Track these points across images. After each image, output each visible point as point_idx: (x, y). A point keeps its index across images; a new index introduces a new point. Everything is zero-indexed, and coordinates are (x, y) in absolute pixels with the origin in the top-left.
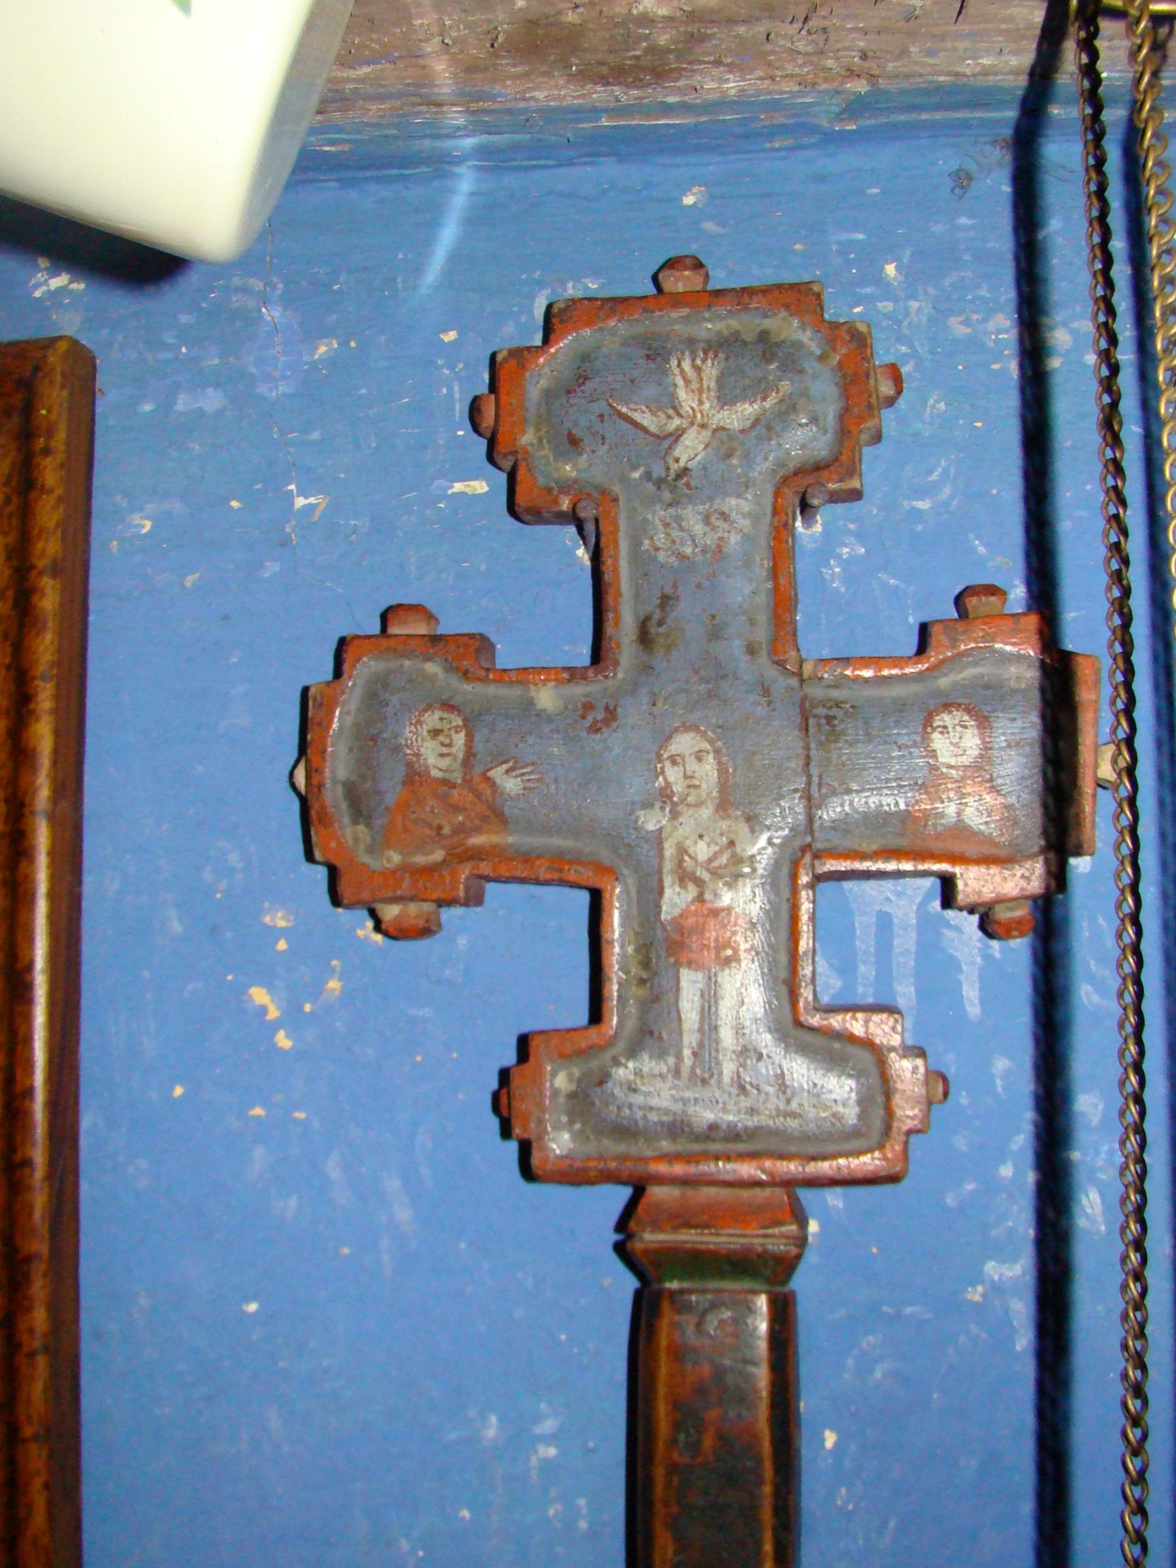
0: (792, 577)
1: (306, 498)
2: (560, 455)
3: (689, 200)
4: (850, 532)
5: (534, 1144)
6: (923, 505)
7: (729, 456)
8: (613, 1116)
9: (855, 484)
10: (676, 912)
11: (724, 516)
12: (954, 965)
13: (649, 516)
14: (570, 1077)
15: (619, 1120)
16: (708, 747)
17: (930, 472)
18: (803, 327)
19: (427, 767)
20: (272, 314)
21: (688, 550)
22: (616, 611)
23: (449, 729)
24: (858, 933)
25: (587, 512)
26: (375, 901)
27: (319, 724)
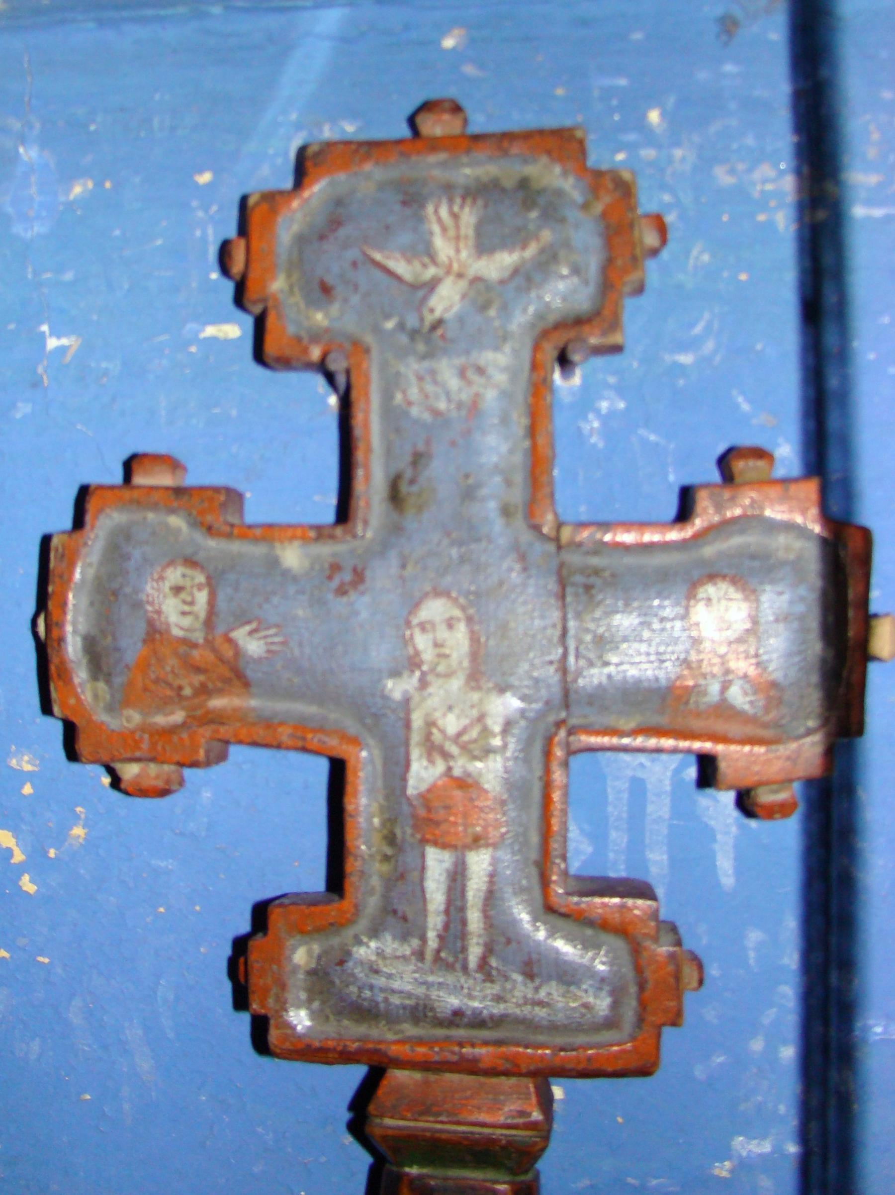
0: (551, 436)
1: (59, 337)
2: (312, 304)
3: (449, 43)
4: (609, 386)
5: (272, 1022)
6: (685, 359)
7: (485, 307)
8: (354, 997)
9: (616, 338)
10: (424, 787)
11: (481, 371)
12: (709, 834)
13: (402, 369)
14: (310, 953)
15: (360, 1001)
16: (457, 613)
17: (692, 325)
18: (565, 173)
19: (168, 625)
20: (28, 154)
21: (442, 405)
22: (367, 468)
23: (192, 587)
24: (611, 798)
25: (337, 364)
26: (113, 760)
27: (61, 576)
